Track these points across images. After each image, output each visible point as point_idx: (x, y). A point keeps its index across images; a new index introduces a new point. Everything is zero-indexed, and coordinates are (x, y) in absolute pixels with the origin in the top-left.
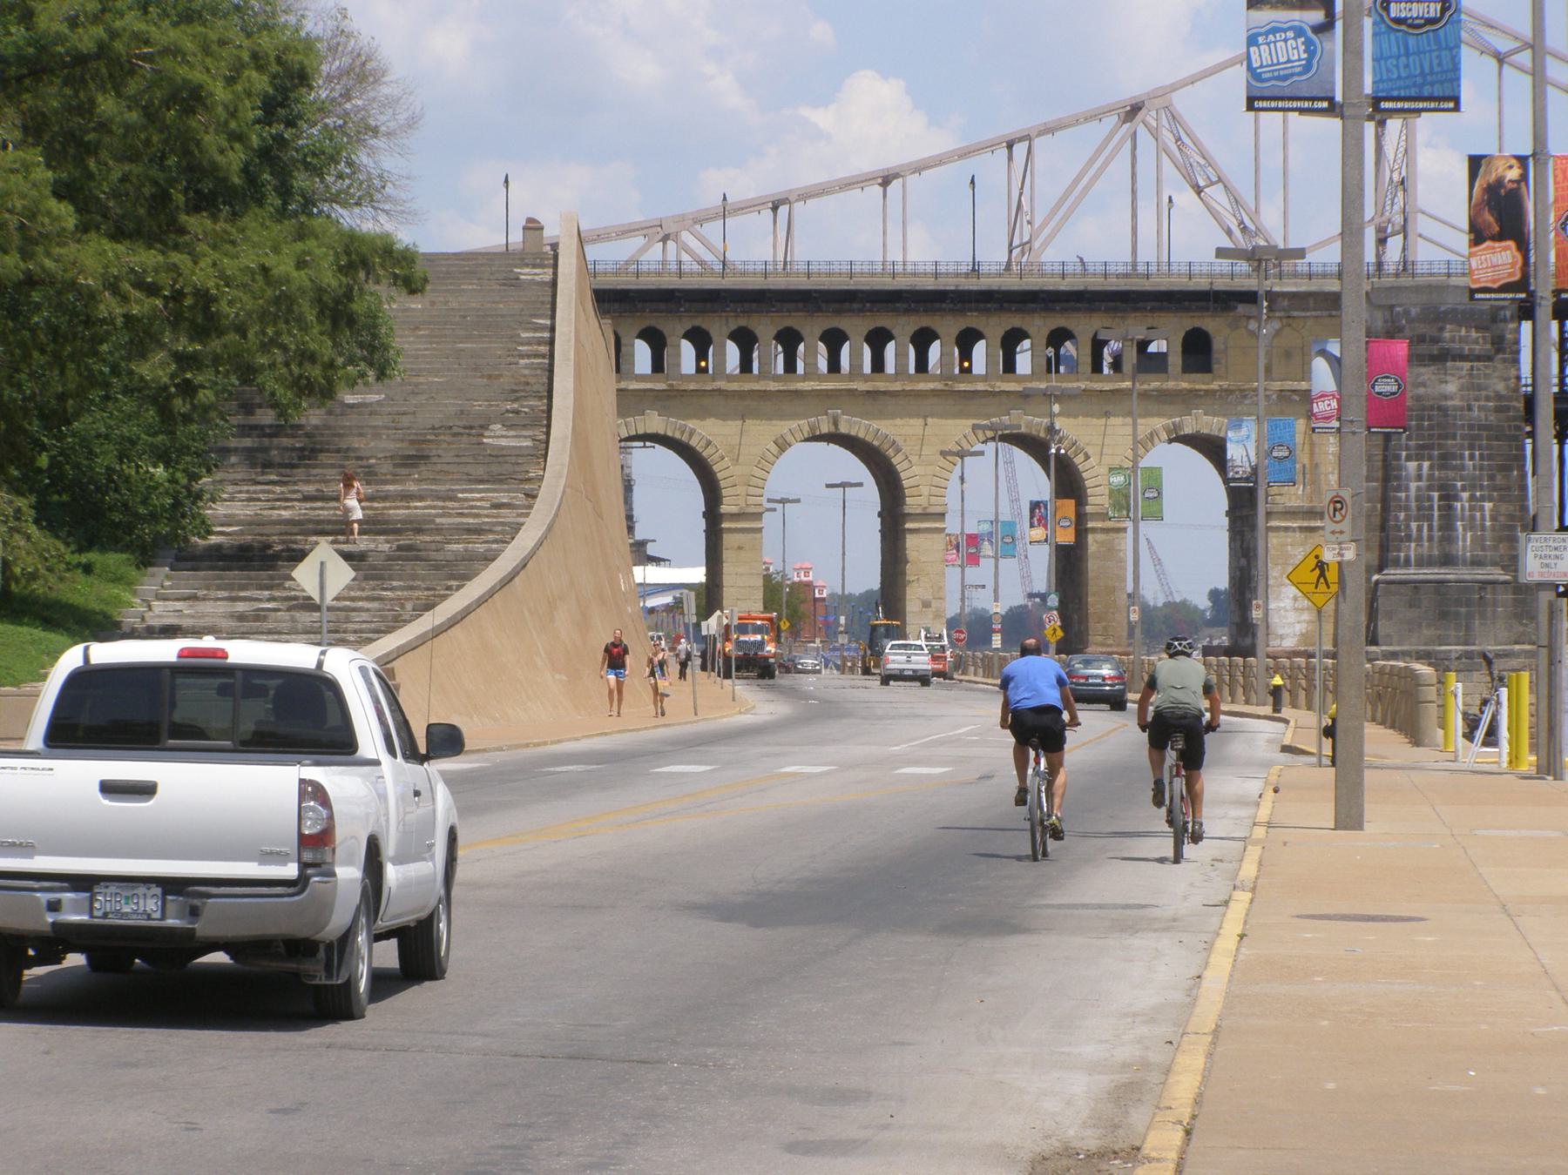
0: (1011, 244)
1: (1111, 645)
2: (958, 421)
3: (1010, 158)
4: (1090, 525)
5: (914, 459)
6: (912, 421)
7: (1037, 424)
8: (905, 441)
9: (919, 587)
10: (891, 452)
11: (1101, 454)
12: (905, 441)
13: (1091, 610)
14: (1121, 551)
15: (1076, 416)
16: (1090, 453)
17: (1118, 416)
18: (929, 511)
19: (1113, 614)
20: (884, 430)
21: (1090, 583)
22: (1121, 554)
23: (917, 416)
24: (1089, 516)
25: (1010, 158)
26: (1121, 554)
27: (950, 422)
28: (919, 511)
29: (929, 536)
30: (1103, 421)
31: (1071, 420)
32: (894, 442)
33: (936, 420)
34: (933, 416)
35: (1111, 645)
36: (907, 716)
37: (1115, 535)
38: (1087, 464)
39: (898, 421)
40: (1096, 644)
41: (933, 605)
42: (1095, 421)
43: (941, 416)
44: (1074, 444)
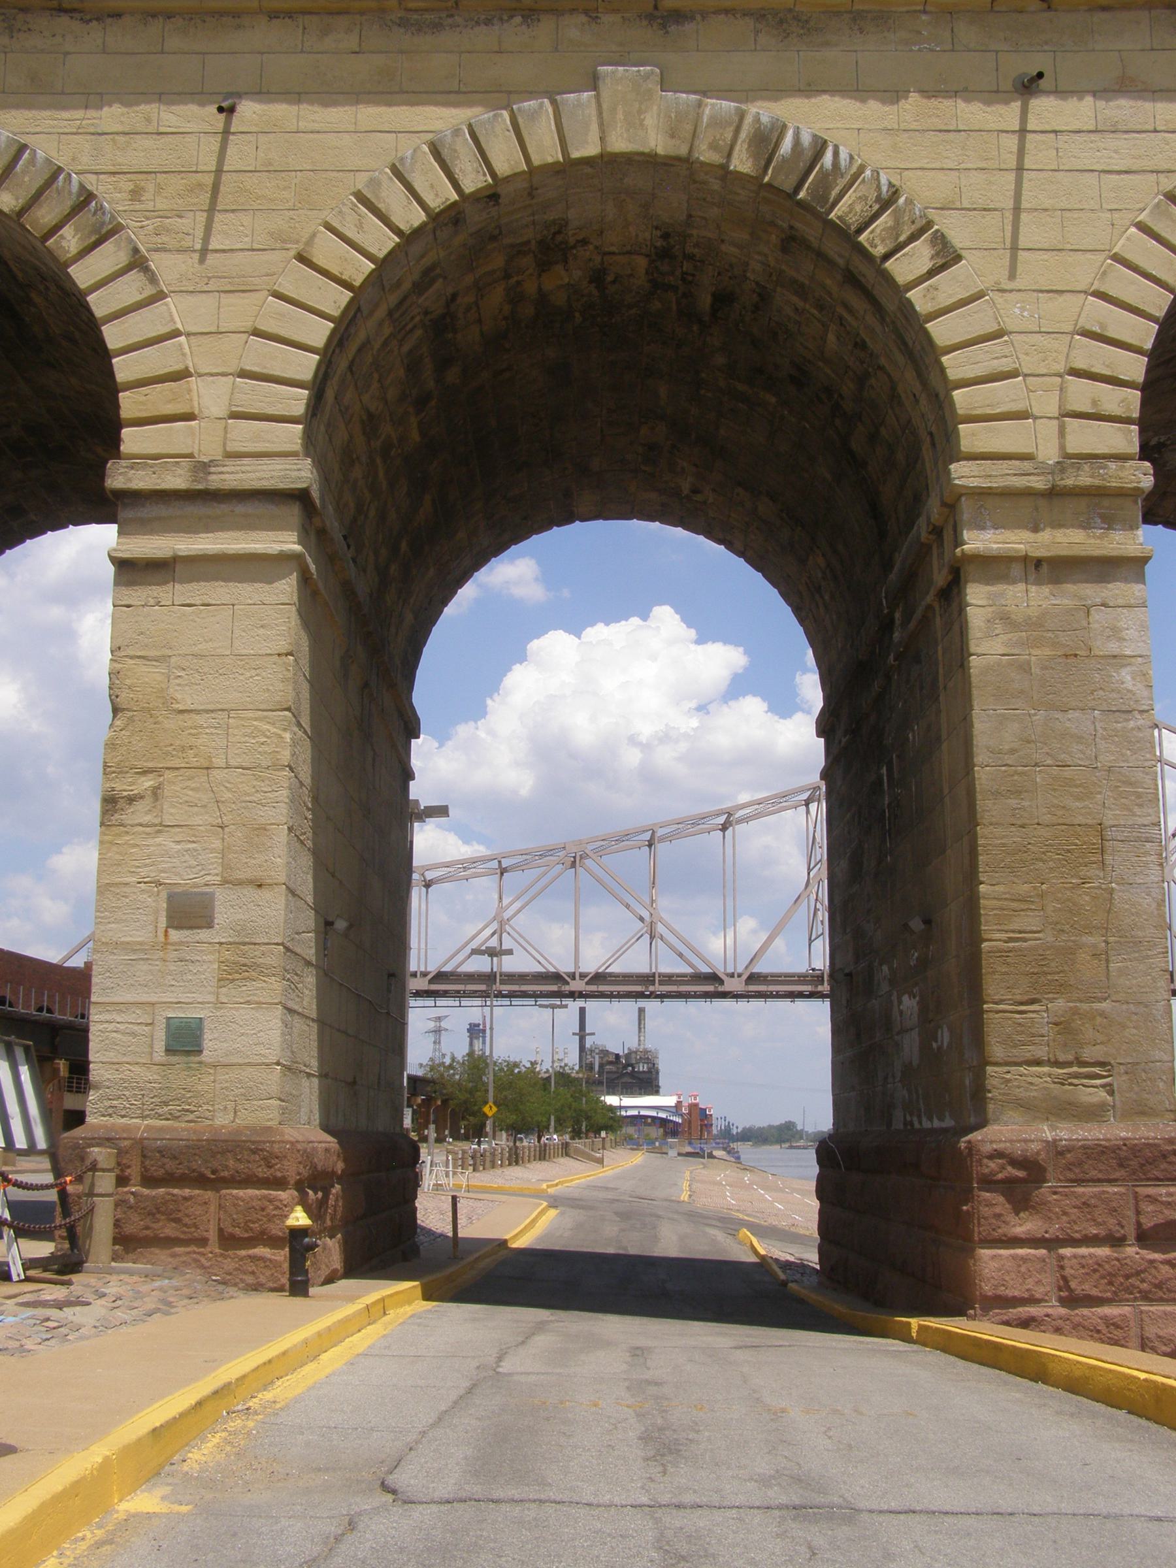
0: (810, 939)
1: (1094, 1113)
2: (370, 114)
3: (808, 812)
4: (976, 541)
5: (166, 267)
6: (171, 116)
7: (717, 122)
8: (136, 194)
9: (161, 828)
10: (69, 240)
11: (1015, 248)
12: (136, 194)
13: (993, 938)
14: (1117, 659)
15: (893, 94)
16: (958, 238)
17: (1079, 93)
18: (216, 481)
19: (1103, 956)
20: (45, 149)
21: (988, 808)
22: (1126, 676)
23: (196, 95)
24: (966, 509)
25: (808, 812)
26: (1126, 676)
27: (339, 115)
28: (177, 480)
29: (219, 591)
30: (1008, 114)
31: (873, 105)
32: (86, 198)
33: (281, 111)
34: (261, 93)
35: (1094, 1113)
36: (900, 1513)
37: (1091, 592)
38: (949, 286)
39: (112, 116)
40: (1026, 1107)
41: (223, 915)
42: (972, 113)
43: (295, 95)
44: (886, 204)
